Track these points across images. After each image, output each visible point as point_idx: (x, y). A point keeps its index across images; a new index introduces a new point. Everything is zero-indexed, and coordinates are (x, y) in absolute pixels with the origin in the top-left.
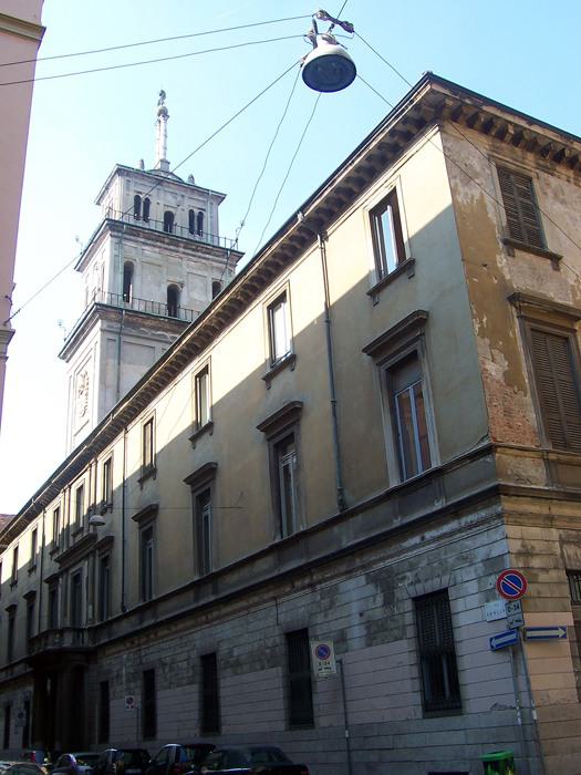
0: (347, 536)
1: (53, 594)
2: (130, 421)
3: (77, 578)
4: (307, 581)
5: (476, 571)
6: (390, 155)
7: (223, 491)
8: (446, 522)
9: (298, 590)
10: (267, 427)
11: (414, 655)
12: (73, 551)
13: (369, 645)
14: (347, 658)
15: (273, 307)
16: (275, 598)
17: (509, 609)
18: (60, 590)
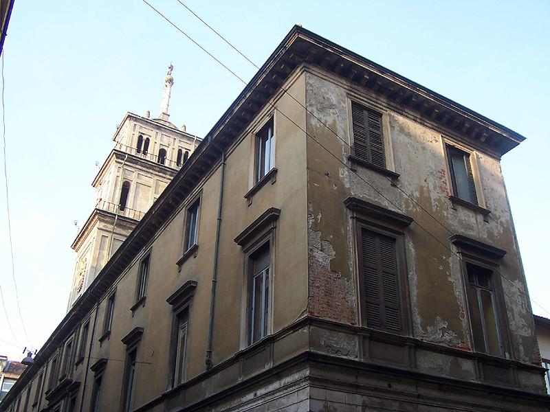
6: (271, 91)
8: (271, 382)
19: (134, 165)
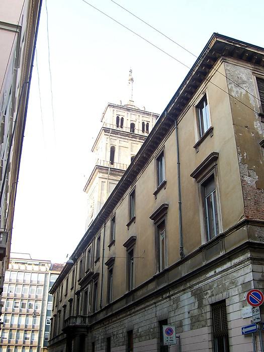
0: (184, 271)
1: (78, 300)
2: (106, 218)
3: (86, 293)
4: (168, 295)
5: (238, 290)
8: (225, 263)
11: (210, 336)
12: (86, 279)
13: (191, 329)
14: (182, 335)
17: (253, 312)
19: (116, 136)
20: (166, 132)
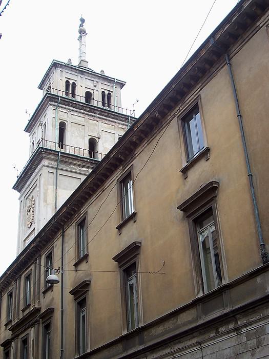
3: (25, 342)
7: (145, 263)
9: (223, 334)
10: (119, 259)
15: (186, 119)
16: (200, 343)
18: (12, 350)
19: (67, 107)
20: (141, 141)
